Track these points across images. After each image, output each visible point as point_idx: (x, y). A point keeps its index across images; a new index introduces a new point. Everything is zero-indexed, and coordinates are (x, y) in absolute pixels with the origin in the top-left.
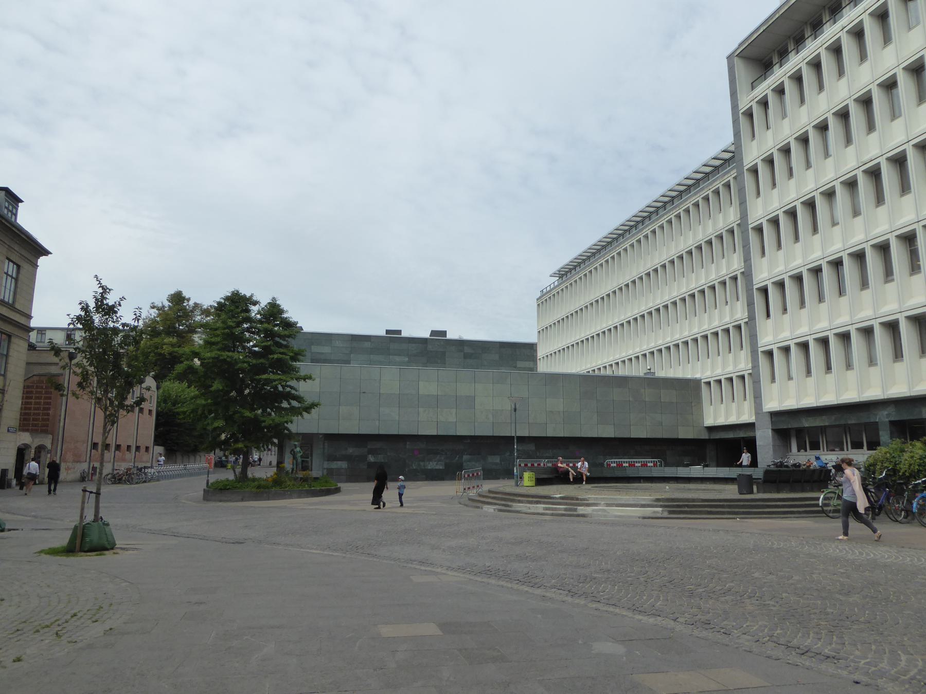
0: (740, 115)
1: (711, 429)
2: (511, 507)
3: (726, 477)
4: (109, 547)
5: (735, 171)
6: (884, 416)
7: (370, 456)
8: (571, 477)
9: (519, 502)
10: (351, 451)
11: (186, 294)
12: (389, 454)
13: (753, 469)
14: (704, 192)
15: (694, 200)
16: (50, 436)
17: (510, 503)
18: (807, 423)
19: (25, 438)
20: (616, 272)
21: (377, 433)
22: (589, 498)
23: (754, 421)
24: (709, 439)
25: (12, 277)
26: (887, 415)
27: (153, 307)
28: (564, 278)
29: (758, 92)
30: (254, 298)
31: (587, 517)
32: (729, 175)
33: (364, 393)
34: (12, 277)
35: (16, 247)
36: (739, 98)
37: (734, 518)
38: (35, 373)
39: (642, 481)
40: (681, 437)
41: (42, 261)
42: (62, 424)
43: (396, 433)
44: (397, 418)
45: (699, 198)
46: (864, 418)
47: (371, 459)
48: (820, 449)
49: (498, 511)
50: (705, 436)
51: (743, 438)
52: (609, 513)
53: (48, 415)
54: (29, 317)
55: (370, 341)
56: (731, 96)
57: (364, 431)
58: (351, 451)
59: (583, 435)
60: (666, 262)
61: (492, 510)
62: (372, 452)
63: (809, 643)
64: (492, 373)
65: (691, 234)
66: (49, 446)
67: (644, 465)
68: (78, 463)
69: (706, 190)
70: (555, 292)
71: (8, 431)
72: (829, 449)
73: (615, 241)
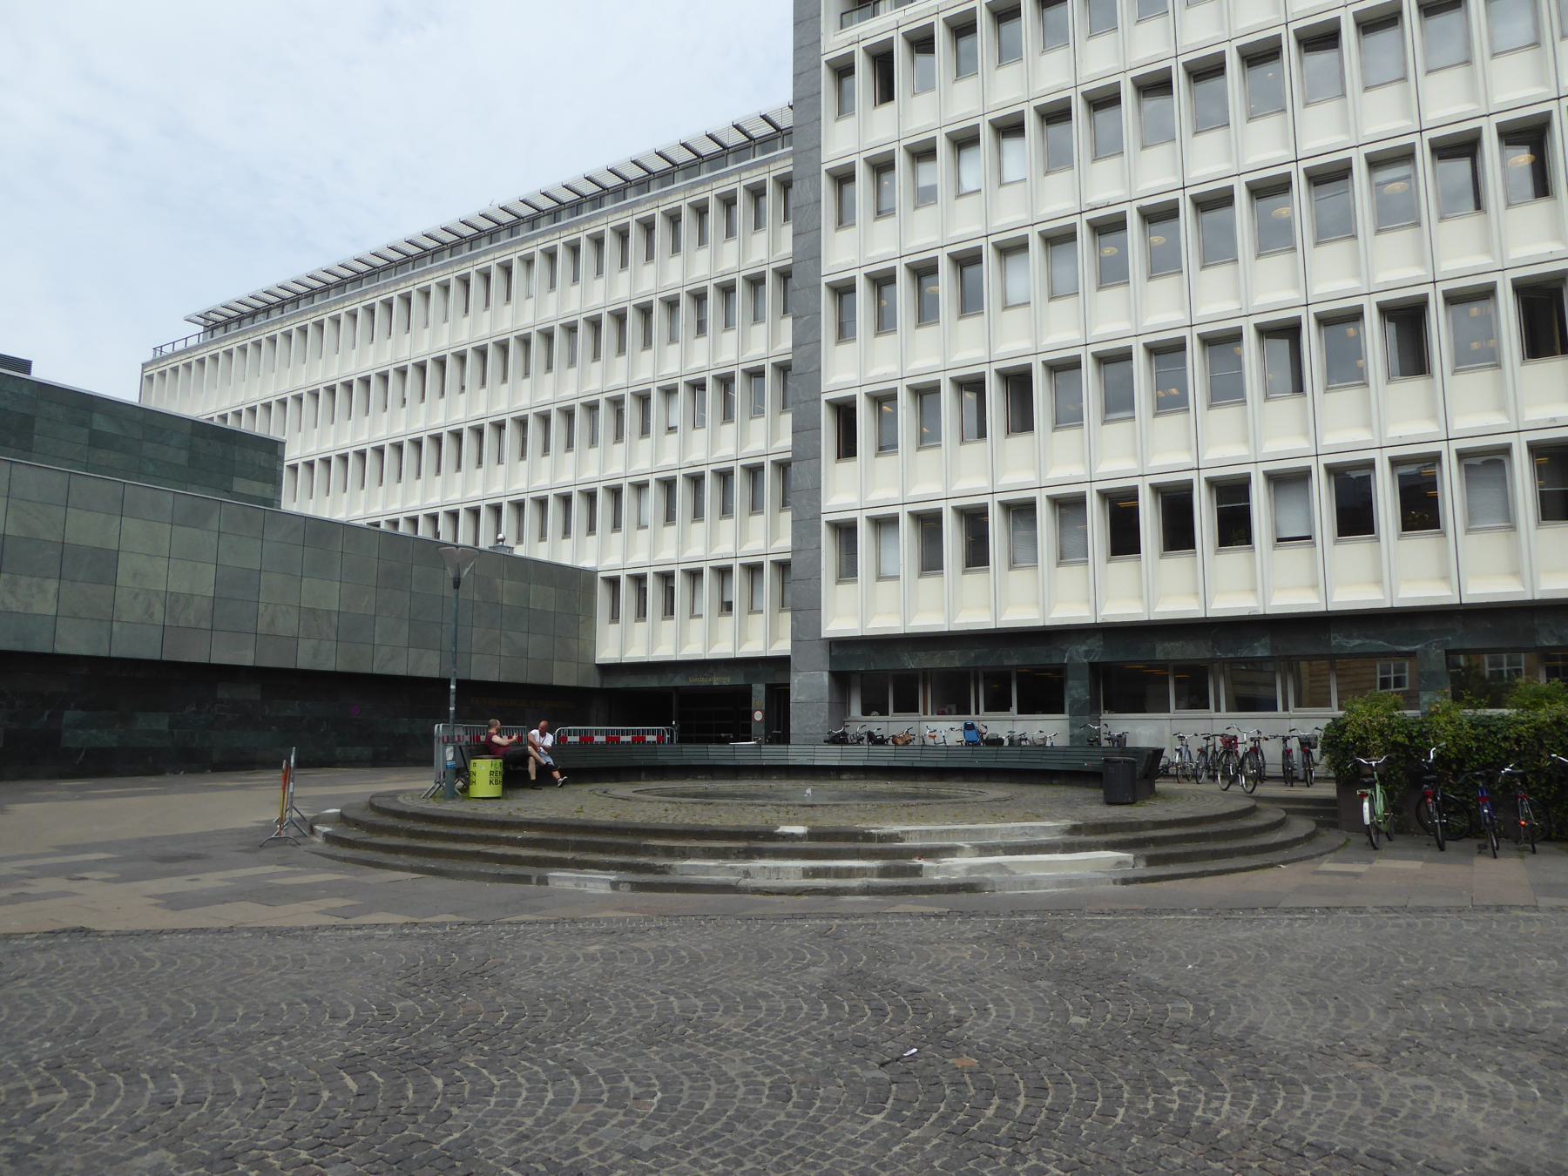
0: (823, 65)
1: (607, 669)
2: (666, 873)
3: (916, 765)
5: (790, 161)
6: (1078, 654)
8: (532, 768)
9: (684, 854)
13: (995, 748)
14: (570, 232)
15: (543, 243)
17: (661, 862)
18: (911, 662)
20: (191, 394)
22: (902, 832)
23: (789, 654)
24: (600, 689)
26: (1086, 651)
28: (219, 334)
29: (871, 29)
31: (981, 891)
32: (376, 294)
36: (822, 31)
37: (1271, 866)
39: (643, 775)
40: (557, 681)
45: (559, 242)
46: (1039, 656)
48: (1207, 707)
49: (633, 890)
50: (594, 682)
51: (676, 688)
52: (1014, 873)
56: (798, 23)
59: (377, 669)
60: (373, 374)
61: (604, 889)
63: (989, 1119)
64: (122, 486)
65: (304, 371)
67: (638, 739)
69: (469, 264)
70: (179, 362)
73: (466, 246)
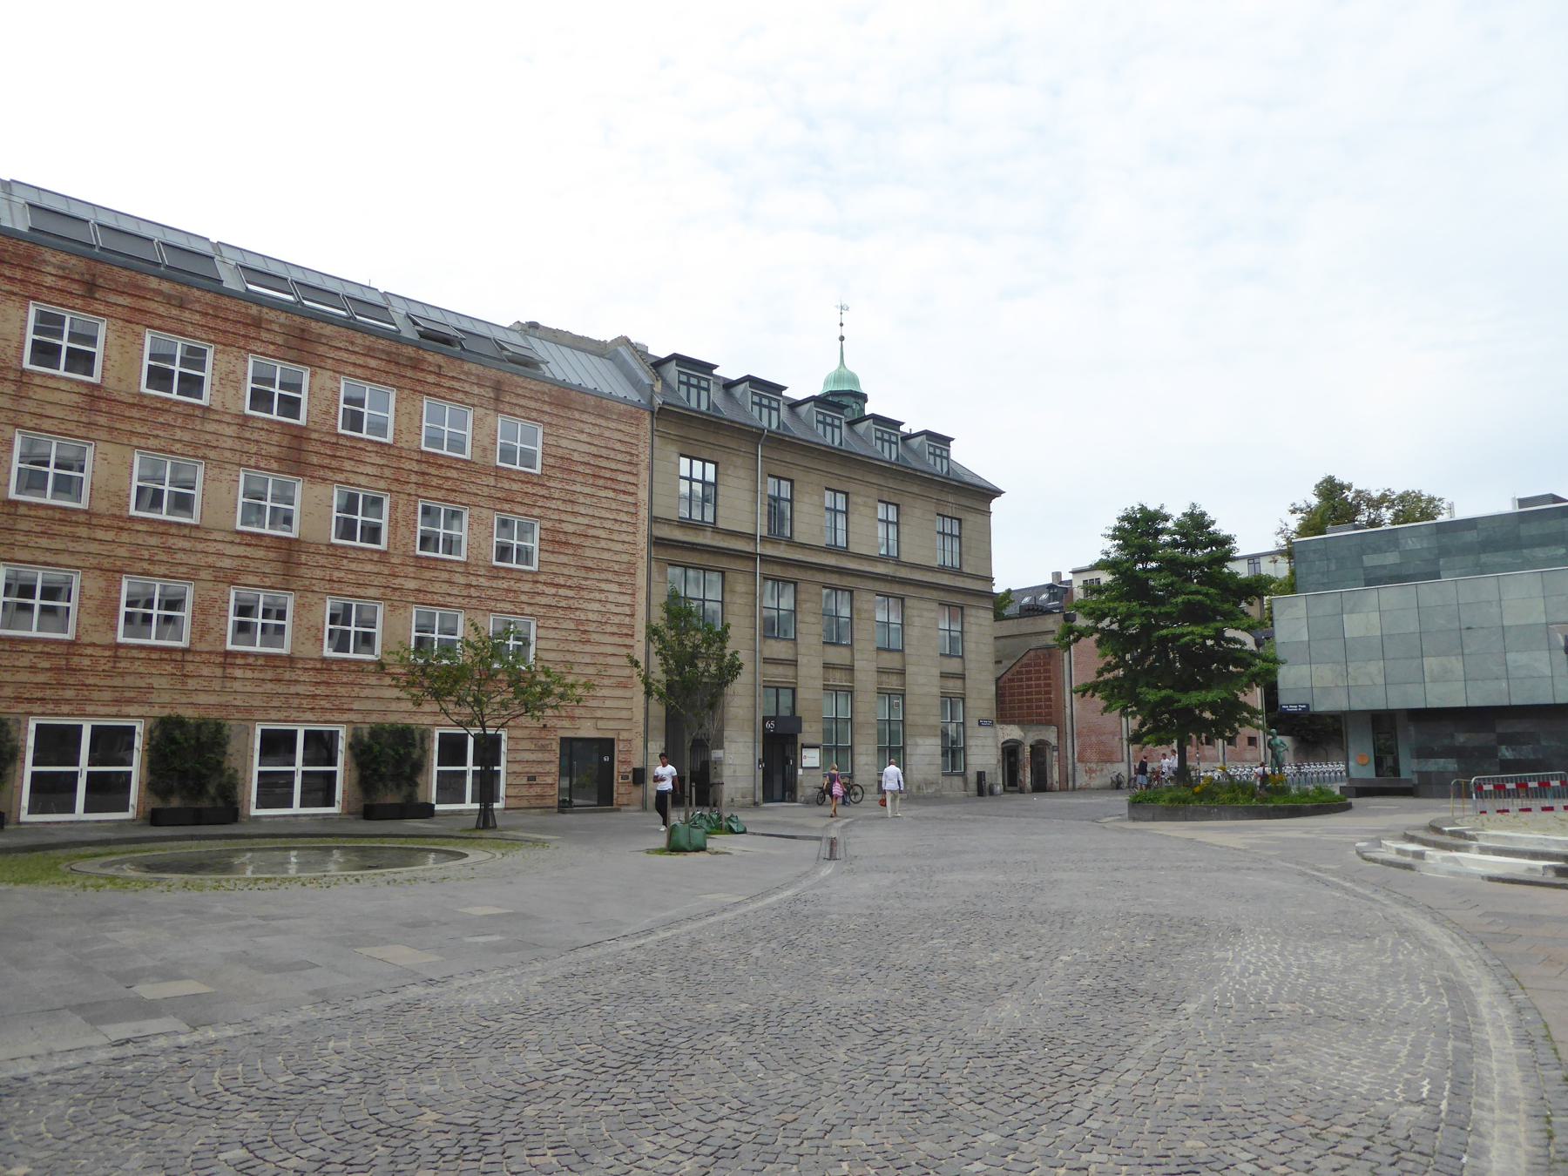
4: (689, 849)
7: (1503, 748)
10: (1461, 739)
11: (1341, 478)
12: (1544, 743)
16: (1054, 729)
19: (1013, 732)
21: (1505, 702)
25: (952, 535)
27: (1293, 512)
30: (1164, 511)
33: (1468, 628)
34: (952, 535)
35: (951, 499)
38: (1033, 646)
41: (995, 505)
42: (1068, 711)
43: (1549, 701)
44: (1548, 672)
47: (1507, 754)
53: (1050, 699)
54: (990, 580)
55: (1476, 528)
57: (1476, 701)
58: (1461, 739)
62: (1506, 740)
64: (1339, 595)
66: (1054, 741)
68: (1108, 765)
71: (980, 724)
72: (122, 754)
